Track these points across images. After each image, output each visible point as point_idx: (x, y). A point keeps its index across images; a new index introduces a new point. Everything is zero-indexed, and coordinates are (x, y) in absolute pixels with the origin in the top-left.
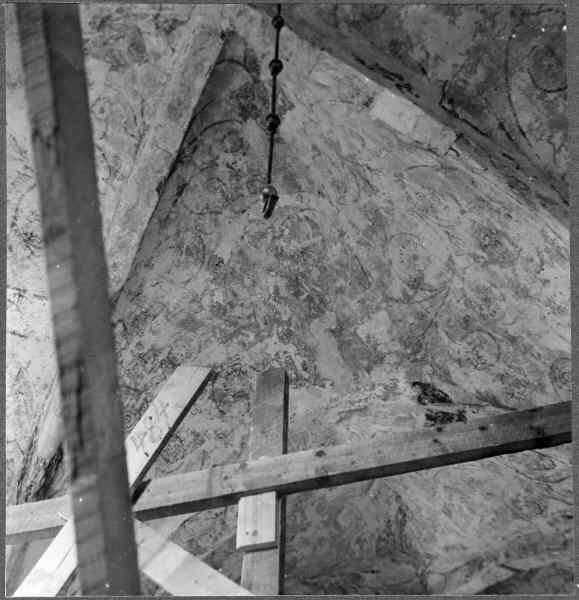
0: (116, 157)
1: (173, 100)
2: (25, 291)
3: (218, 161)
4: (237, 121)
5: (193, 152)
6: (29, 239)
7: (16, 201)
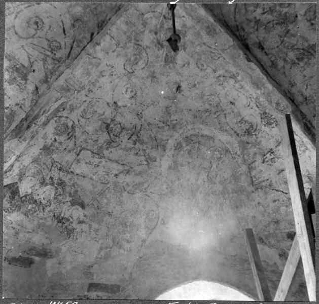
2: (271, 149)
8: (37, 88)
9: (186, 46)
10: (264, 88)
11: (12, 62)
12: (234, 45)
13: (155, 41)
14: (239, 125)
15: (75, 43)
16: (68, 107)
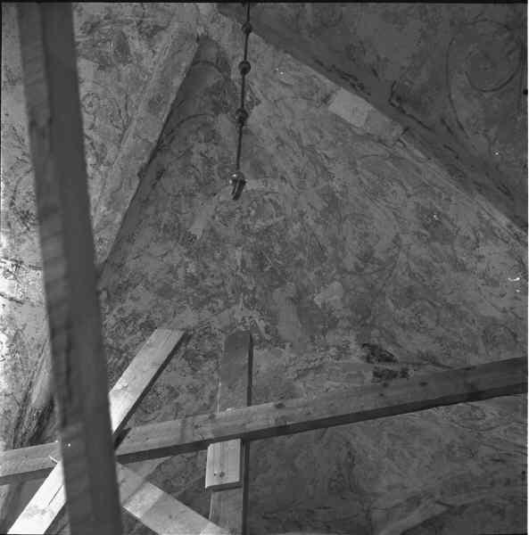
2: (21, 262)
3: (194, 150)
9: (107, 69)
10: (113, 213)
12: (151, 144)
13: (96, 20)
14: (28, 199)
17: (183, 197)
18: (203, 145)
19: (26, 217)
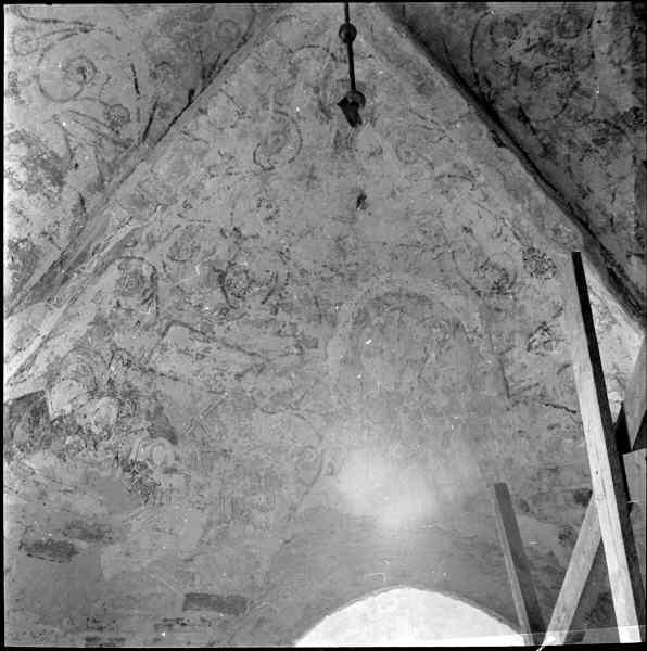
0: (455, 166)
1: (414, 84)
2: (544, 323)
3: (516, 59)
4: (482, 17)
5: (489, 84)
6: (499, 288)
7: (459, 278)
8: (82, 201)
11: (34, 147)
13: (315, 104)
15: (158, 110)
16: (144, 237)
17: (571, 100)
18: (517, 42)
19: (499, 288)
